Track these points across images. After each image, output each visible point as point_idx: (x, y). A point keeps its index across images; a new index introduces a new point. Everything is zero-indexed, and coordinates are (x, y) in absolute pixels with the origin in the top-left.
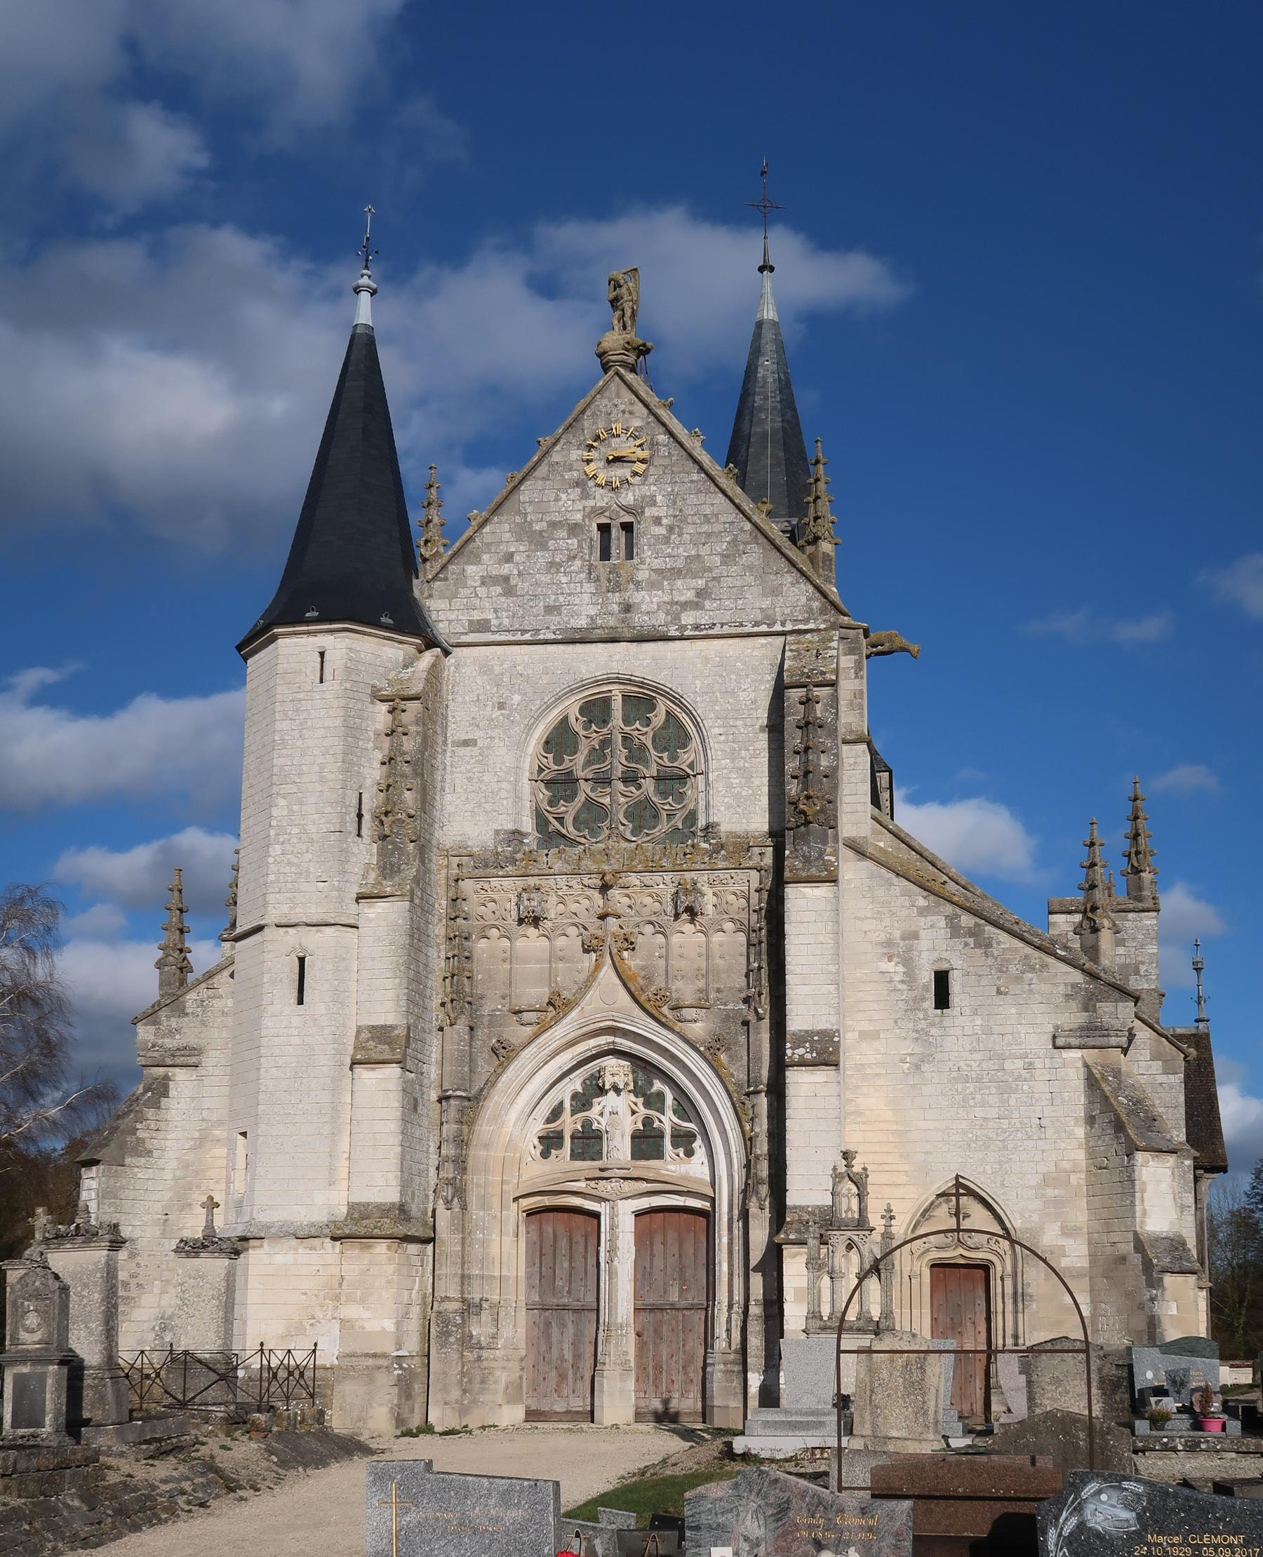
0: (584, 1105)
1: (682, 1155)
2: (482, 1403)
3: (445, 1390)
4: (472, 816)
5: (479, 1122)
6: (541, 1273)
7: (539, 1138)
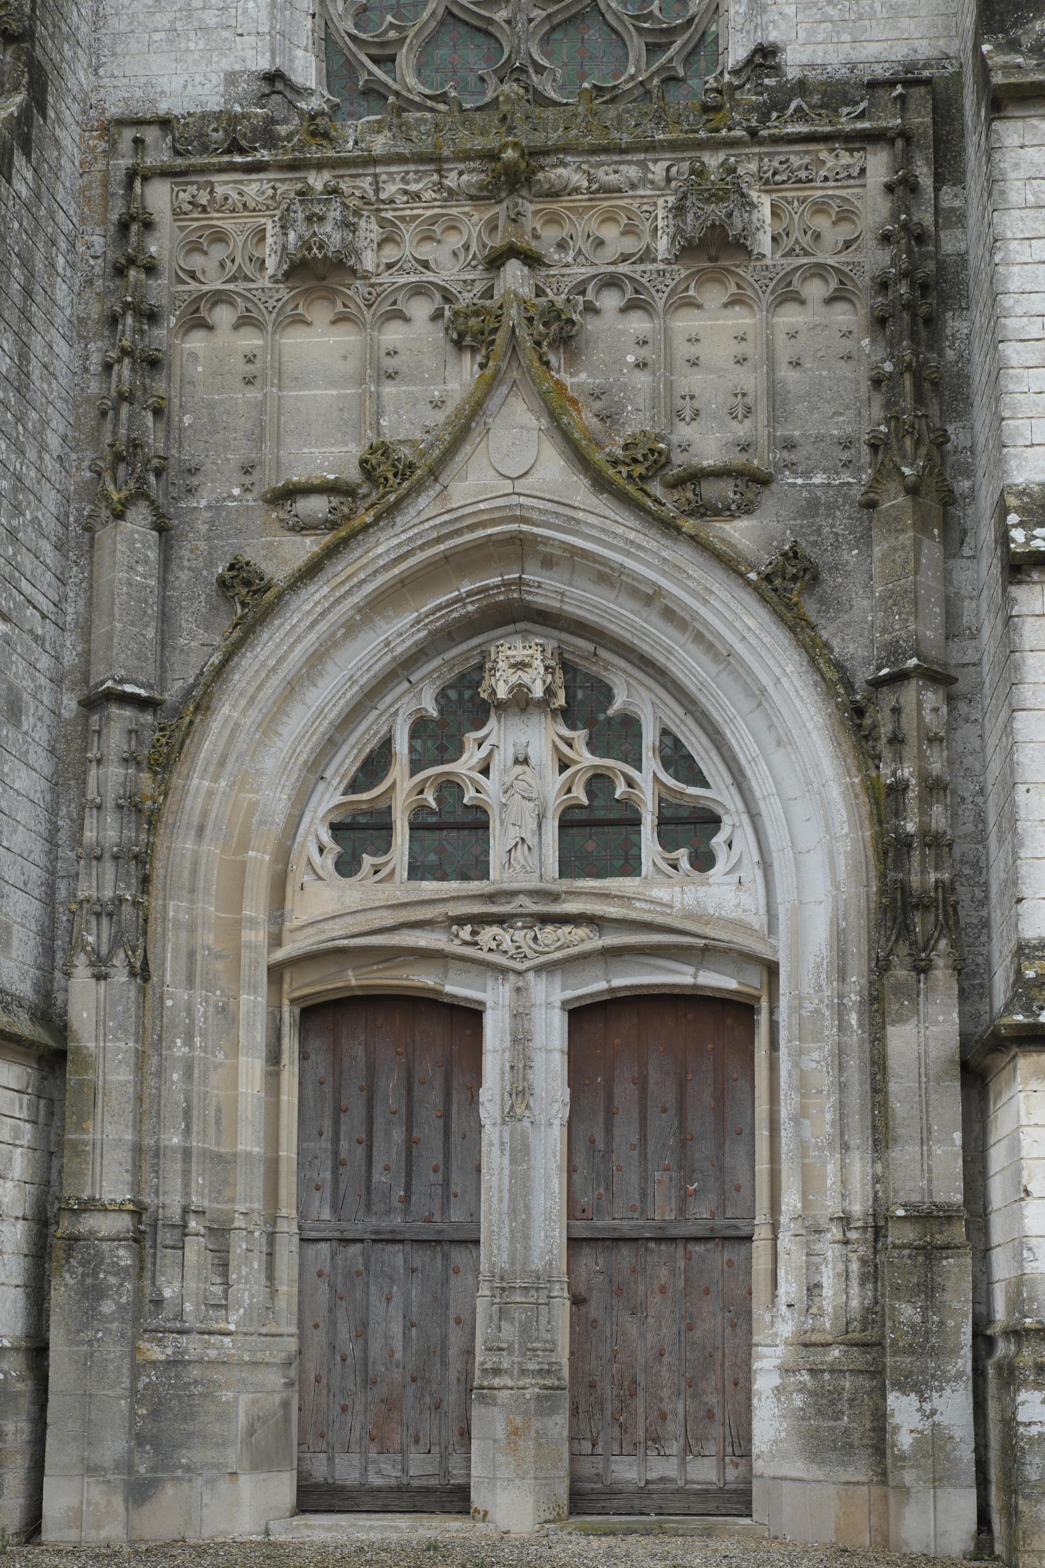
0: (442, 749)
1: (685, 864)
2: (187, 1469)
3: (88, 1436)
4: (170, 42)
5: (182, 768)
6: (336, 1153)
7: (335, 827)
